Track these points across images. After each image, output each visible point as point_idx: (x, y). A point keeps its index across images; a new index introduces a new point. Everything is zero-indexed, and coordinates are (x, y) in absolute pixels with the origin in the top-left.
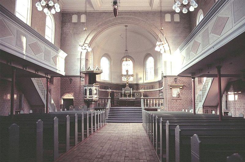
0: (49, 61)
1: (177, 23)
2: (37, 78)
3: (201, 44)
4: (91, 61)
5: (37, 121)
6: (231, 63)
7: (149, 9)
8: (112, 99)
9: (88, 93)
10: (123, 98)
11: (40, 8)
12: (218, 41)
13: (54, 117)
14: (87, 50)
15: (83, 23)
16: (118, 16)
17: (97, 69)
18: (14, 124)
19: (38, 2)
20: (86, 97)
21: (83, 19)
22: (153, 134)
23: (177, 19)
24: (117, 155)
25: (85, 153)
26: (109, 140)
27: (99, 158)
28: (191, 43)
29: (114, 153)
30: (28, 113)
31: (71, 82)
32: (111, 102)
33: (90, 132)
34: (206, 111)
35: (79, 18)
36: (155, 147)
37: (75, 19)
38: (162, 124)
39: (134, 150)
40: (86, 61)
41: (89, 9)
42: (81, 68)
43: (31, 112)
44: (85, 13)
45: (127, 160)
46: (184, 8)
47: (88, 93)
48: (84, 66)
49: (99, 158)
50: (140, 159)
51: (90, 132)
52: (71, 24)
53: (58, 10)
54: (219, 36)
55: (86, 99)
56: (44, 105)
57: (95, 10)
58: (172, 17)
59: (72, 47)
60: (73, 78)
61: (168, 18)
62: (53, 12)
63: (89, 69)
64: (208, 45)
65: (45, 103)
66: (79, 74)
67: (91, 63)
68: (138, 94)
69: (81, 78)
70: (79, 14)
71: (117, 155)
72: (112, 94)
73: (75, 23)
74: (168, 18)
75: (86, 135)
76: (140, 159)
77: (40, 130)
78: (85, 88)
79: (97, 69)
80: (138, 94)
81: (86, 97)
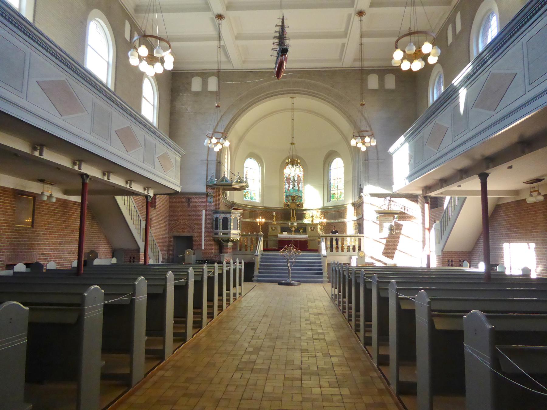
0: (153, 164)
1: (391, 91)
2: (126, 197)
3: (449, 131)
4: (226, 165)
5: (136, 279)
6: (511, 167)
7: (338, 65)
8: (266, 237)
9: (221, 226)
10: (285, 235)
11: (134, 61)
12: (490, 122)
13: (168, 271)
14: (222, 144)
15: (211, 93)
16: (281, 79)
17: (239, 181)
18: (93, 287)
19: (132, 50)
20: (217, 234)
21: (213, 84)
22: (353, 305)
23: (391, 82)
24: (285, 347)
25: (224, 342)
26: (265, 316)
27: (251, 353)
28: (427, 130)
29: (279, 343)
30: (108, 263)
32: (264, 241)
33: (228, 300)
34: (448, 261)
35: (205, 84)
36: (357, 330)
37: (196, 85)
38: (378, 286)
39: (316, 336)
40: (217, 165)
41: (224, 67)
42: (209, 178)
43: (114, 261)
44: (219, 74)
45: (306, 357)
46: (207, 139)
47: (221, 226)
48: (214, 175)
49: (251, 353)
50: (331, 356)
51: (228, 300)
52: (189, 94)
53: (169, 65)
54: (494, 113)
55: (217, 236)
56: (138, 250)
57: (235, 68)
58: (382, 81)
59: (45, 198)
60: (193, 198)
61: (373, 82)
62: (158, 68)
63: (224, 180)
64: (467, 131)
65: (142, 245)
66: (203, 189)
67: (226, 169)
68: (312, 229)
69: (209, 198)
70: (204, 75)
71: (285, 347)
72: (265, 227)
73: (197, 94)
74: (373, 82)
75: (220, 307)
76: (331, 356)
77: (142, 298)
78: (215, 216)
79: (239, 181)
80: (312, 229)
81: (217, 234)
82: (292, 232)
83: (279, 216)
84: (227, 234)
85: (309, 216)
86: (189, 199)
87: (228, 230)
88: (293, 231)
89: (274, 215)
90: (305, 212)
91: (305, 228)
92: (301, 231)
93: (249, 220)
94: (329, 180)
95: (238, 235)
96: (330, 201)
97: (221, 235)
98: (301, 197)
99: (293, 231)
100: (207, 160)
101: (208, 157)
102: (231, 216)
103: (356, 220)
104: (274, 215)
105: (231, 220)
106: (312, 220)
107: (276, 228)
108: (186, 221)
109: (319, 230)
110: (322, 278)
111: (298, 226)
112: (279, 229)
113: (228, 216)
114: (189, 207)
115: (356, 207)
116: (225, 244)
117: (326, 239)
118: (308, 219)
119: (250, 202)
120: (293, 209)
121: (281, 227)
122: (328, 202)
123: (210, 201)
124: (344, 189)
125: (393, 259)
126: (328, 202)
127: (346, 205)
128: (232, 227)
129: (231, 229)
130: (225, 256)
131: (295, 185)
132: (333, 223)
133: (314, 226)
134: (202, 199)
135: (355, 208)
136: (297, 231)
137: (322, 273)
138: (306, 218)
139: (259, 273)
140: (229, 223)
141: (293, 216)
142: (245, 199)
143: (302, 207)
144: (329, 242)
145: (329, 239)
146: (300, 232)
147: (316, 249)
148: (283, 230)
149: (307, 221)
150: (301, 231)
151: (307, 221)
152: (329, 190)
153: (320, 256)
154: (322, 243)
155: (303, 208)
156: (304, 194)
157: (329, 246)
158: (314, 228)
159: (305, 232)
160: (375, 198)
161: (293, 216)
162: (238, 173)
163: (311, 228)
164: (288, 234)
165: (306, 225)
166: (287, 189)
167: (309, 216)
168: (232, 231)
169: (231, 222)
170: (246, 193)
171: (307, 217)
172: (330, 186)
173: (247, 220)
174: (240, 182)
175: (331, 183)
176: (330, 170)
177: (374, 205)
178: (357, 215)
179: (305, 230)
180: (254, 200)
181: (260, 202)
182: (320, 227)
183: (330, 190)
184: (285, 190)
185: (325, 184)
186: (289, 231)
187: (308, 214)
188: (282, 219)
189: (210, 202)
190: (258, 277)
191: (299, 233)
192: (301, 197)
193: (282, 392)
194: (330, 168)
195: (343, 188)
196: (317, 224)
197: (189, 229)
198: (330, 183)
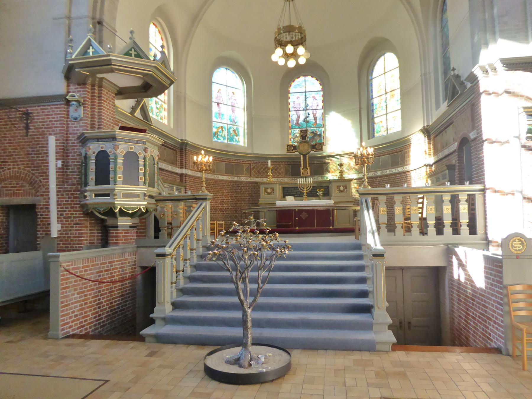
10: (291, 202)
17: (133, 52)
31: (27, 128)
60: (34, 110)
68: (342, 188)
80: (342, 188)
82: (302, 196)
83: (282, 170)
84: (108, 195)
85: (335, 168)
86: (27, 115)
87: (109, 184)
88: (305, 194)
89: (269, 165)
90: (328, 160)
91: (328, 187)
92: (320, 193)
93: (225, 178)
94: (370, 98)
95: (141, 196)
96: (374, 136)
97: (91, 199)
98: (320, 135)
99: (305, 194)
100: (69, 18)
101: (70, 11)
102: (116, 147)
103: (434, 164)
104: (269, 165)
105: (116, 158)
106: (341, 172)
107: (273, 189)
108: (22, 167)
109: (354, 191)
110: (368, 327)
111: (315, 185)
112: (279, 191)
113: (107, 146)
114: (27, 132)
115: (432, 137)
116: (110, 221)
117: (374, 200)
118: (333, 174)
119: (227, 145)
120: (304, 153)
121: (284, 189)
122: (369, 139)
123: (76, 115)
124: (402, 109)
125: (453, 234)
126: (369, 139)
127: (406, 137)
128: (120, 175)
129: (115, 182)
130: (61, 259)
131: (309, 114)
132: (381, 176)
133: (344, 183)
134: (57, 111)
135: (429, 139)
136: (313, 194)
137: (367, 309)
138: (329, 172)
139: (176, 306)
140: (112, 166)
141: (305, 166)
142: (216, 139)
143: (321, 150)
144: (383, 210)
145: (382, 199)
146: (318, 196)
147: (116, 226)
148: (287, 192)
149: (330, 176)
150: (320, 193)
151: (330, 176)
152: (371, 117)
153: (358, 247)
154: (366, 212)
155: (325, 154)
156: (325, 129)
157: (384, 219)
158: (345, 187)
159: (327, 194)
160: (520, 73)
161: (305, 166)
162: (132, 32)
163: (338, 187)
164: (295, 200)
165: (330, 182)
166: (295, 122)
167: (335, 168)
168: (120, 188)
169: (116, 163)
170: (218, 128)
171: (332, 170)
172: (373, 110)
173: (221, 177)
174: (138, 56)
175: (374, 103)
176: (372, 79)
177: (517, 96)
178: (436, 152)
179: (328, 191)
180: (235, 143)
181: (246, 146)
182: (356, 185)
183: (373, 116)
184: (290, 125)
185: (362, 106)
186: (296, 192)
187: (333, 165)
188: (287, 174)
189: (76, 119)
190: (168, 321)
191: (317, 198)
192: (320, 135)
193: (385, 92)
194: (372, 76)
195: (399, 107)
196: (350, 180)
197: (27, 187)
198: (373, 104)
